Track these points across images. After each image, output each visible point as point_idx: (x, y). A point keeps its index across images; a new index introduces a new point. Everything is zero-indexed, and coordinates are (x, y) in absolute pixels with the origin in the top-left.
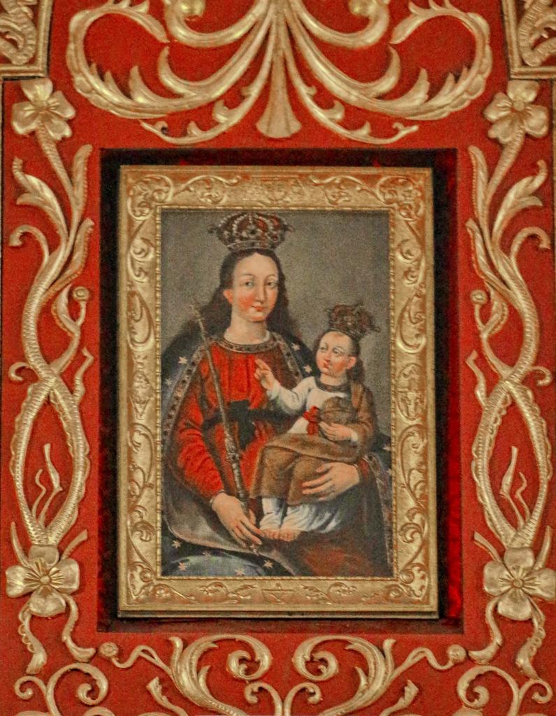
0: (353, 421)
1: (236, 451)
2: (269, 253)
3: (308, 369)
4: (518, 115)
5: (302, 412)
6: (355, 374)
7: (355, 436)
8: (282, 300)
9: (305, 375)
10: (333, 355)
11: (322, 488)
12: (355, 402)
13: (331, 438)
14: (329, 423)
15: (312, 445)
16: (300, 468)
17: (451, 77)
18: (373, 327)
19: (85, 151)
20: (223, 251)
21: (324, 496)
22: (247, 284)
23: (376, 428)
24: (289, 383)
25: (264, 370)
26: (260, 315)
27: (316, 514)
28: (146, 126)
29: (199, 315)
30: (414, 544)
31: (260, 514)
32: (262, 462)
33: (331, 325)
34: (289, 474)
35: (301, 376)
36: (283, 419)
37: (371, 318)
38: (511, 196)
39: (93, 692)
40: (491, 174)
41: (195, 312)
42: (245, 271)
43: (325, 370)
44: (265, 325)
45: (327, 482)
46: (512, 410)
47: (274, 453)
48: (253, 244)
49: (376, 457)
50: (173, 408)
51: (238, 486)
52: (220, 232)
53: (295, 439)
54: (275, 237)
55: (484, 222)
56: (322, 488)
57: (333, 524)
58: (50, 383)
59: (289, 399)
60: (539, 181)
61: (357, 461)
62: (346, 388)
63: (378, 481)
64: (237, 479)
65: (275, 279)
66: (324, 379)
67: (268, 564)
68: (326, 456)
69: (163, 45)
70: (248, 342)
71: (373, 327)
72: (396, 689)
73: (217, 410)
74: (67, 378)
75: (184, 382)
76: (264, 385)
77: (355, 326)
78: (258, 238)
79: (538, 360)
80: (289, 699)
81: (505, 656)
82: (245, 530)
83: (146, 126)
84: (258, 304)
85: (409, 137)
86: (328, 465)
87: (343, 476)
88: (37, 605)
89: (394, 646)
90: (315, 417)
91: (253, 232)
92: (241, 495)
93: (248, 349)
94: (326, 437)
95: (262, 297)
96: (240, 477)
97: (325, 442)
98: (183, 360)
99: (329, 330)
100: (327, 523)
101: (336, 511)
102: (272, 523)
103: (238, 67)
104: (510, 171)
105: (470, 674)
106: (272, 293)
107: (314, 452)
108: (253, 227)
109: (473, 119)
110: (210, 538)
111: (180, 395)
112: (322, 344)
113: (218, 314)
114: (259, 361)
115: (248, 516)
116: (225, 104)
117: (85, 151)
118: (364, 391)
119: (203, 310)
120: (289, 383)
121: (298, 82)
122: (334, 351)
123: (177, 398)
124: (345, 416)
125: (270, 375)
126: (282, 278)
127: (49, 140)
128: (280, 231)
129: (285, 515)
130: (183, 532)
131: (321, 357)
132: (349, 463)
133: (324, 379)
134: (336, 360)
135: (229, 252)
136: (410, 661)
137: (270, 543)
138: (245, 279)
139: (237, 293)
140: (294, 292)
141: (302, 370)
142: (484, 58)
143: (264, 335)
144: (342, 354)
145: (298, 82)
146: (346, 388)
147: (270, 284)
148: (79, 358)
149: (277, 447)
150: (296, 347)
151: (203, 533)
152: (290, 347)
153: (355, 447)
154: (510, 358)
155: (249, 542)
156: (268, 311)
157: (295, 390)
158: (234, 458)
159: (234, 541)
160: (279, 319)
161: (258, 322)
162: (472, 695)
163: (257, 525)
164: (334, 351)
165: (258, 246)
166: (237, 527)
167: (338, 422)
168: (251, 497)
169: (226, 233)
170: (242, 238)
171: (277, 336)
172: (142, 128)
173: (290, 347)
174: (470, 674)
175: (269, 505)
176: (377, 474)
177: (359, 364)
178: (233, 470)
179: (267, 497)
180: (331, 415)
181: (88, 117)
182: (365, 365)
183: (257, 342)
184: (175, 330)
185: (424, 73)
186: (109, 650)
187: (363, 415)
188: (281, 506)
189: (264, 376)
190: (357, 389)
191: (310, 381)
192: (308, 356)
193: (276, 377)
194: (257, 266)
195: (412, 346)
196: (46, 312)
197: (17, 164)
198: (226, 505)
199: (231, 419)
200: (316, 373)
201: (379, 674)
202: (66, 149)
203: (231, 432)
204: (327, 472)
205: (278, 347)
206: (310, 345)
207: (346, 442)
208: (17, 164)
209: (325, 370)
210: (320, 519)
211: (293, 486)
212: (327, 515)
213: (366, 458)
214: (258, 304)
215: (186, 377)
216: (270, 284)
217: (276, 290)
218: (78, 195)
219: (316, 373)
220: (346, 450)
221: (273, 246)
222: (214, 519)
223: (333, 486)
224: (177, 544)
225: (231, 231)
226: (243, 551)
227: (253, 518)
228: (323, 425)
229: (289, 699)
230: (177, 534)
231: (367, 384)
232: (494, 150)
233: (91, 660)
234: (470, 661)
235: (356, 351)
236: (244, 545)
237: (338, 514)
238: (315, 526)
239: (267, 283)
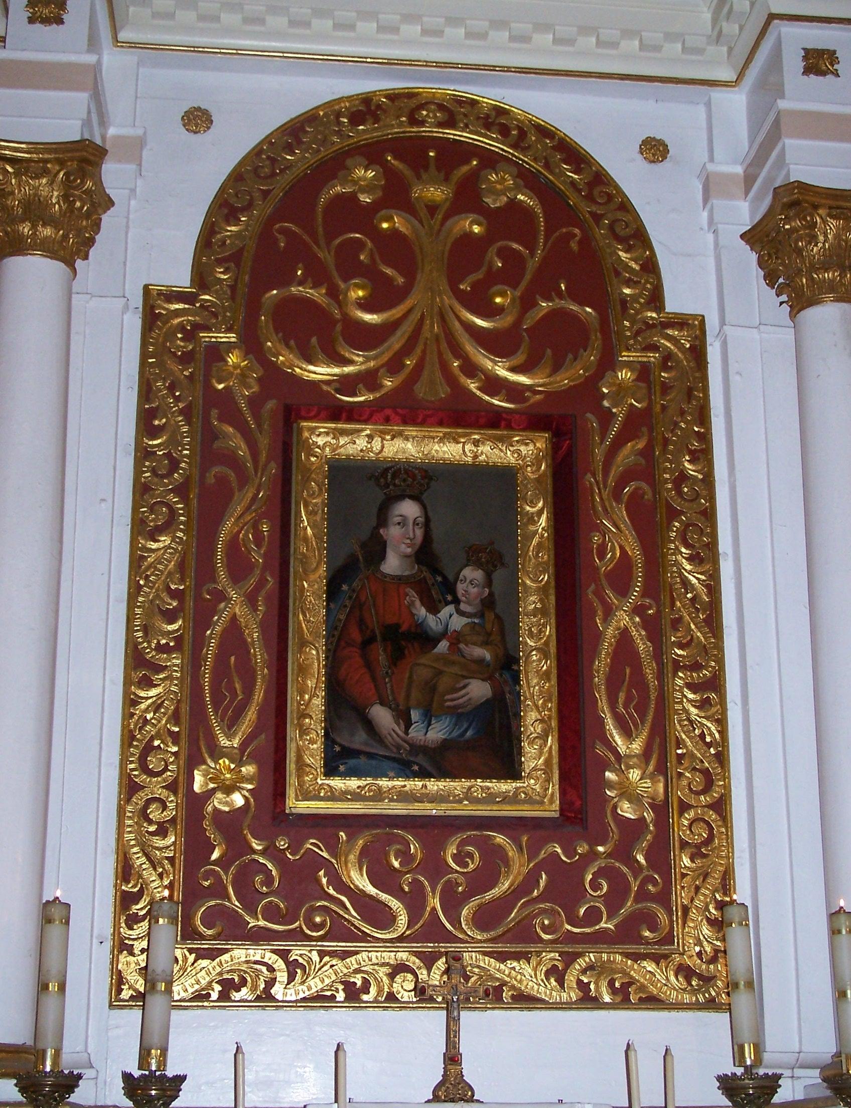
0: (485, 644)
1: (390, 668)
2: (415, 498)
3: (449, 598)
4: (621, 391)
5: (444, 635)
6: (488, 603)
7: (488, 656)
8: (427, 538)
9: (447, 603)
10: (470, 587)
11: (461, 701)
12: (488, 627)
13: (469, 657)
14: (466, 645)
15: (454, 663)
16: (444, 683)
17: (570, 356)
18: (503, 564)
19: (271, 405)
20: (380, 496)
21: (463, 708)
22: (399, 524)
23: (506, 649)
24: (434, 609)
25: (412, 596)
26: (409, 550)
27: (456, 725)
28: (325, 388)
29: (358, 549)
30: (538, 752)
31: (408, 724)
32: (410, 677)
33: (468, 560)
34: (433, 689)
35: (443, 603)
36: (427, 640)
37: (501, 556)
38: (619, 458)
39: (269, 881)
40: (603, 439)
41: (357, 548)
42: (397, 513)
43: (464, 599)
44: (413, 558)
45: (463, 697)
46: (624, 634)
47: (421, 667)
48: (404, 490)
49: (507, 675)
50: (336, 628)
51: (390, 698)
52: (377, 479)
53: (440, 657)
54: (421, 485)
55: (600, 477)
56: (461, 701)
57: (469, 734)
58: (235, 605)
59: (433, 623)
60: (641, 444)
61: (489, 678)
62: (481, 615)
63: (508, 696)
64: (389, 692)
65: (421, 520)
66: (463, 607)
67: (416, 768)
68: (464, 673)
69: (337, 321)
70: (399, 573)
71: (503, 564)
72: (531, 880)
73: (373, 631)
74: (251, 600)
75: (345, 606)
76: (414, 611)
77: (488, 562)
78: (408, 486)
79: (644, 594)
80: (439, 887)
81: (623, 852)
82: (395, 735)
83: (325, 388)
84: (408, 541)
85: (538, 403)
86: (467, 681)
87: (479, 690)
88: (219, 802)
89: (528, 840)
90: (456, 639)
91: (404, 480)
92: (393, 706)
93: (400, 580)
94: (464, 657)
95: (411, 536)
96: (392, 690)
97: (462, 660)
98: (345, 587)
99: (467, 565)
100: (466, 731)
101: (473, 721)
102: (416, 733)
103: (396, 342)
104: (617, 437)
105: (593, 869)
106: (419, 533)
107: (455, 669)
108: (405, 476)
109: (587, 392)
110: (366, 744)
111: (342, 617)
112: (461, 577)
113: (376, 549)
114: (409, 590)
115: (398, 725)
116: (388, 371)
117: (271, 405)
118: (497, 618)
119: (363, 545)
120: (434, 609)
121: (448, 355)
122: (471, 582)
123: (340, 620)
124: (481, 638)
125: (418, 603)
126: (427, 520)
127: (243, 396)
128: (426, 480)
129: (429, 724)
130: (344, 739)
131: (460, 588)
132: (483, 680)
133: (463, 607)
134: (474, 591)
135: (384, 497)
136: (542, 855)
137: (417, 749)
138: (398, 519)
139: (393, 533)
140: (437, 532)
141: (445, 599)
142: (596, 340)
143: (413, 568)
144: (477, 586)
145: (448, 355)
146: (481, 615)
147: (418, 524)
148: (262, 582)
149: (425, 665)
150: (439, 579)
151: (359, 740)
152: (435, 578)
153: (488, 666)
154: (623, 591)
155: (399, 747)
156: (417, 547)
157: (438, 615)
158: (387, 673)
159: (386, 747)
160: (424, 554)
161: (407, 556)
162: (595, 886)
163: (407, 733)
164: (471, 582)
165: (408, 492)
166: (390, 734)
167: (474, 644)
168: (401, 707)
169: (382, 480)
170: (395, 485)
171: (424, 568)
172: (322, 390)
173: (435, 578)
174: (593, 869)
175: (415, 715)
176: (507, 689)
177: (491, 594)
178: (386, 684)
179: (415, 708)
180: (468, 638)
181: (275, 380)
182: (496, 597)
183: (407, 573)
184: (340, 562)
185: (549, 352)
186: (282, 844)
187: (495, 638)
188: (426, 716)
189: (413, 602)
190: (490, 616)
191: (450, 609)
192: (449, 587)
193: (423, 604)
194: (409, 509)
195: (534, 585)
196: (233, 545)
197: (214, 413)
198: (382, 716)
199: (384, 639)
200: (456, 601)
201: (519, 865)
202: (255, 403)
203: (385, 650)
204: (465, 687)
205: (425, 578)
206: (451, 577)
207: (481, 661)
208: (214, 413)
209: (464, 599)
210: (459, 728)
211: (436, 698)
212: (465, 726)
213: (497, 675)
214: (408, 541)
215: (348, 603)
216: (418, 524)
217: (422, 530)
218: (264, 442)
219: (456, 601)
220: (480, 669)
221: (422, 494)
222: (370, 726)
223: (470, 699)
224: (337, 749)
225: (386, 478)
226: (393, 755)
227: (403, 727)
228: (462, 646)
229: (439, 887)
230: (338, 740)
231: (497, 611)
232: (606, 418)
233: (263, 853)
234: (592, 855)
235: (489, 582)
236: (395, 750)
237: (474, 724)
238: (455, 734)
239: (415, 523)
